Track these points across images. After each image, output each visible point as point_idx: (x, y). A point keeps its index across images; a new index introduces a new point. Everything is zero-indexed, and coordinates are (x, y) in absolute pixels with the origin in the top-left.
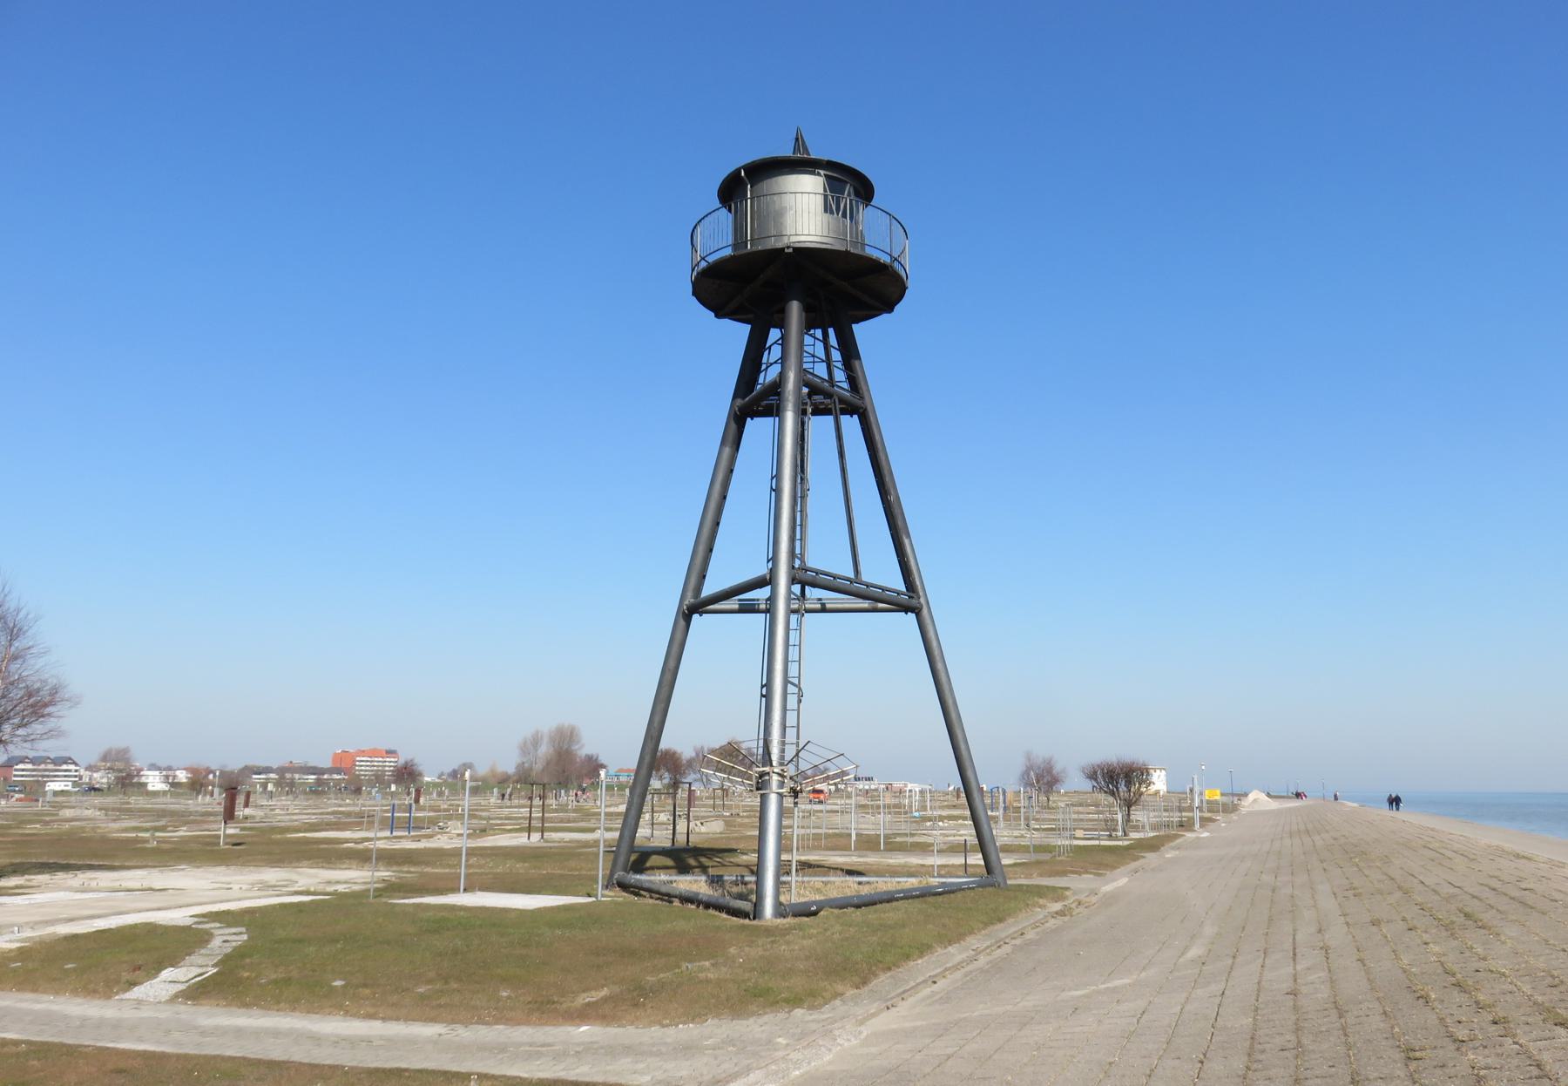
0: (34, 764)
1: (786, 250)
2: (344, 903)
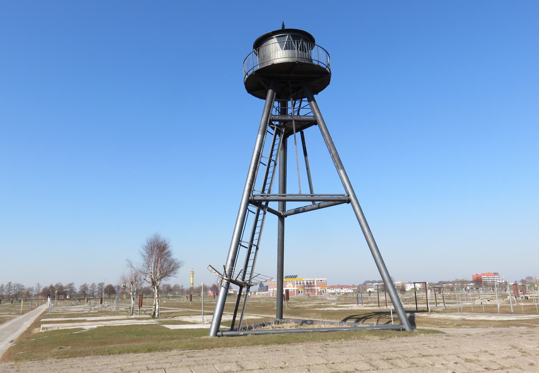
0: (378, 283)
1: (253, 74)
2: (262, 318)
